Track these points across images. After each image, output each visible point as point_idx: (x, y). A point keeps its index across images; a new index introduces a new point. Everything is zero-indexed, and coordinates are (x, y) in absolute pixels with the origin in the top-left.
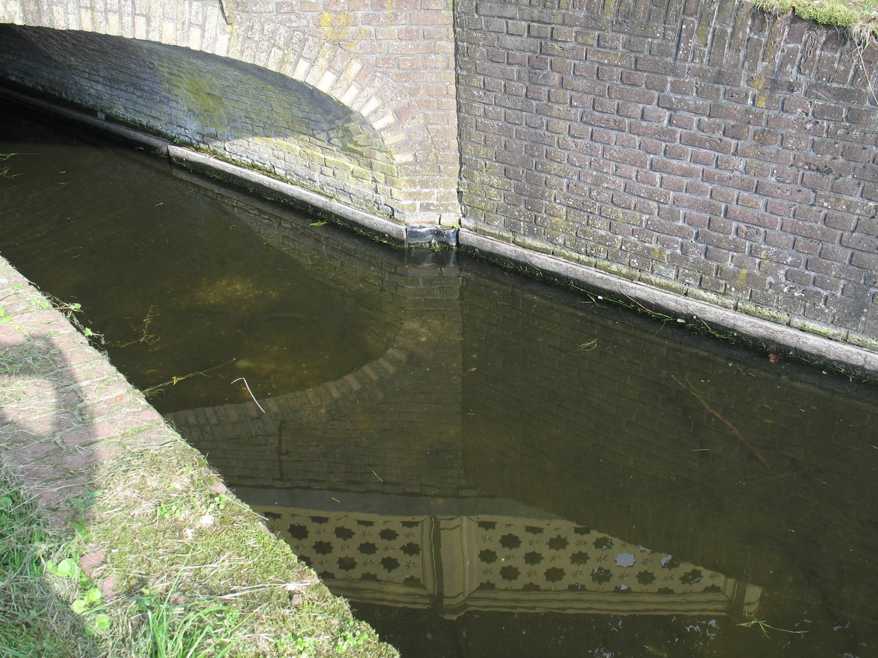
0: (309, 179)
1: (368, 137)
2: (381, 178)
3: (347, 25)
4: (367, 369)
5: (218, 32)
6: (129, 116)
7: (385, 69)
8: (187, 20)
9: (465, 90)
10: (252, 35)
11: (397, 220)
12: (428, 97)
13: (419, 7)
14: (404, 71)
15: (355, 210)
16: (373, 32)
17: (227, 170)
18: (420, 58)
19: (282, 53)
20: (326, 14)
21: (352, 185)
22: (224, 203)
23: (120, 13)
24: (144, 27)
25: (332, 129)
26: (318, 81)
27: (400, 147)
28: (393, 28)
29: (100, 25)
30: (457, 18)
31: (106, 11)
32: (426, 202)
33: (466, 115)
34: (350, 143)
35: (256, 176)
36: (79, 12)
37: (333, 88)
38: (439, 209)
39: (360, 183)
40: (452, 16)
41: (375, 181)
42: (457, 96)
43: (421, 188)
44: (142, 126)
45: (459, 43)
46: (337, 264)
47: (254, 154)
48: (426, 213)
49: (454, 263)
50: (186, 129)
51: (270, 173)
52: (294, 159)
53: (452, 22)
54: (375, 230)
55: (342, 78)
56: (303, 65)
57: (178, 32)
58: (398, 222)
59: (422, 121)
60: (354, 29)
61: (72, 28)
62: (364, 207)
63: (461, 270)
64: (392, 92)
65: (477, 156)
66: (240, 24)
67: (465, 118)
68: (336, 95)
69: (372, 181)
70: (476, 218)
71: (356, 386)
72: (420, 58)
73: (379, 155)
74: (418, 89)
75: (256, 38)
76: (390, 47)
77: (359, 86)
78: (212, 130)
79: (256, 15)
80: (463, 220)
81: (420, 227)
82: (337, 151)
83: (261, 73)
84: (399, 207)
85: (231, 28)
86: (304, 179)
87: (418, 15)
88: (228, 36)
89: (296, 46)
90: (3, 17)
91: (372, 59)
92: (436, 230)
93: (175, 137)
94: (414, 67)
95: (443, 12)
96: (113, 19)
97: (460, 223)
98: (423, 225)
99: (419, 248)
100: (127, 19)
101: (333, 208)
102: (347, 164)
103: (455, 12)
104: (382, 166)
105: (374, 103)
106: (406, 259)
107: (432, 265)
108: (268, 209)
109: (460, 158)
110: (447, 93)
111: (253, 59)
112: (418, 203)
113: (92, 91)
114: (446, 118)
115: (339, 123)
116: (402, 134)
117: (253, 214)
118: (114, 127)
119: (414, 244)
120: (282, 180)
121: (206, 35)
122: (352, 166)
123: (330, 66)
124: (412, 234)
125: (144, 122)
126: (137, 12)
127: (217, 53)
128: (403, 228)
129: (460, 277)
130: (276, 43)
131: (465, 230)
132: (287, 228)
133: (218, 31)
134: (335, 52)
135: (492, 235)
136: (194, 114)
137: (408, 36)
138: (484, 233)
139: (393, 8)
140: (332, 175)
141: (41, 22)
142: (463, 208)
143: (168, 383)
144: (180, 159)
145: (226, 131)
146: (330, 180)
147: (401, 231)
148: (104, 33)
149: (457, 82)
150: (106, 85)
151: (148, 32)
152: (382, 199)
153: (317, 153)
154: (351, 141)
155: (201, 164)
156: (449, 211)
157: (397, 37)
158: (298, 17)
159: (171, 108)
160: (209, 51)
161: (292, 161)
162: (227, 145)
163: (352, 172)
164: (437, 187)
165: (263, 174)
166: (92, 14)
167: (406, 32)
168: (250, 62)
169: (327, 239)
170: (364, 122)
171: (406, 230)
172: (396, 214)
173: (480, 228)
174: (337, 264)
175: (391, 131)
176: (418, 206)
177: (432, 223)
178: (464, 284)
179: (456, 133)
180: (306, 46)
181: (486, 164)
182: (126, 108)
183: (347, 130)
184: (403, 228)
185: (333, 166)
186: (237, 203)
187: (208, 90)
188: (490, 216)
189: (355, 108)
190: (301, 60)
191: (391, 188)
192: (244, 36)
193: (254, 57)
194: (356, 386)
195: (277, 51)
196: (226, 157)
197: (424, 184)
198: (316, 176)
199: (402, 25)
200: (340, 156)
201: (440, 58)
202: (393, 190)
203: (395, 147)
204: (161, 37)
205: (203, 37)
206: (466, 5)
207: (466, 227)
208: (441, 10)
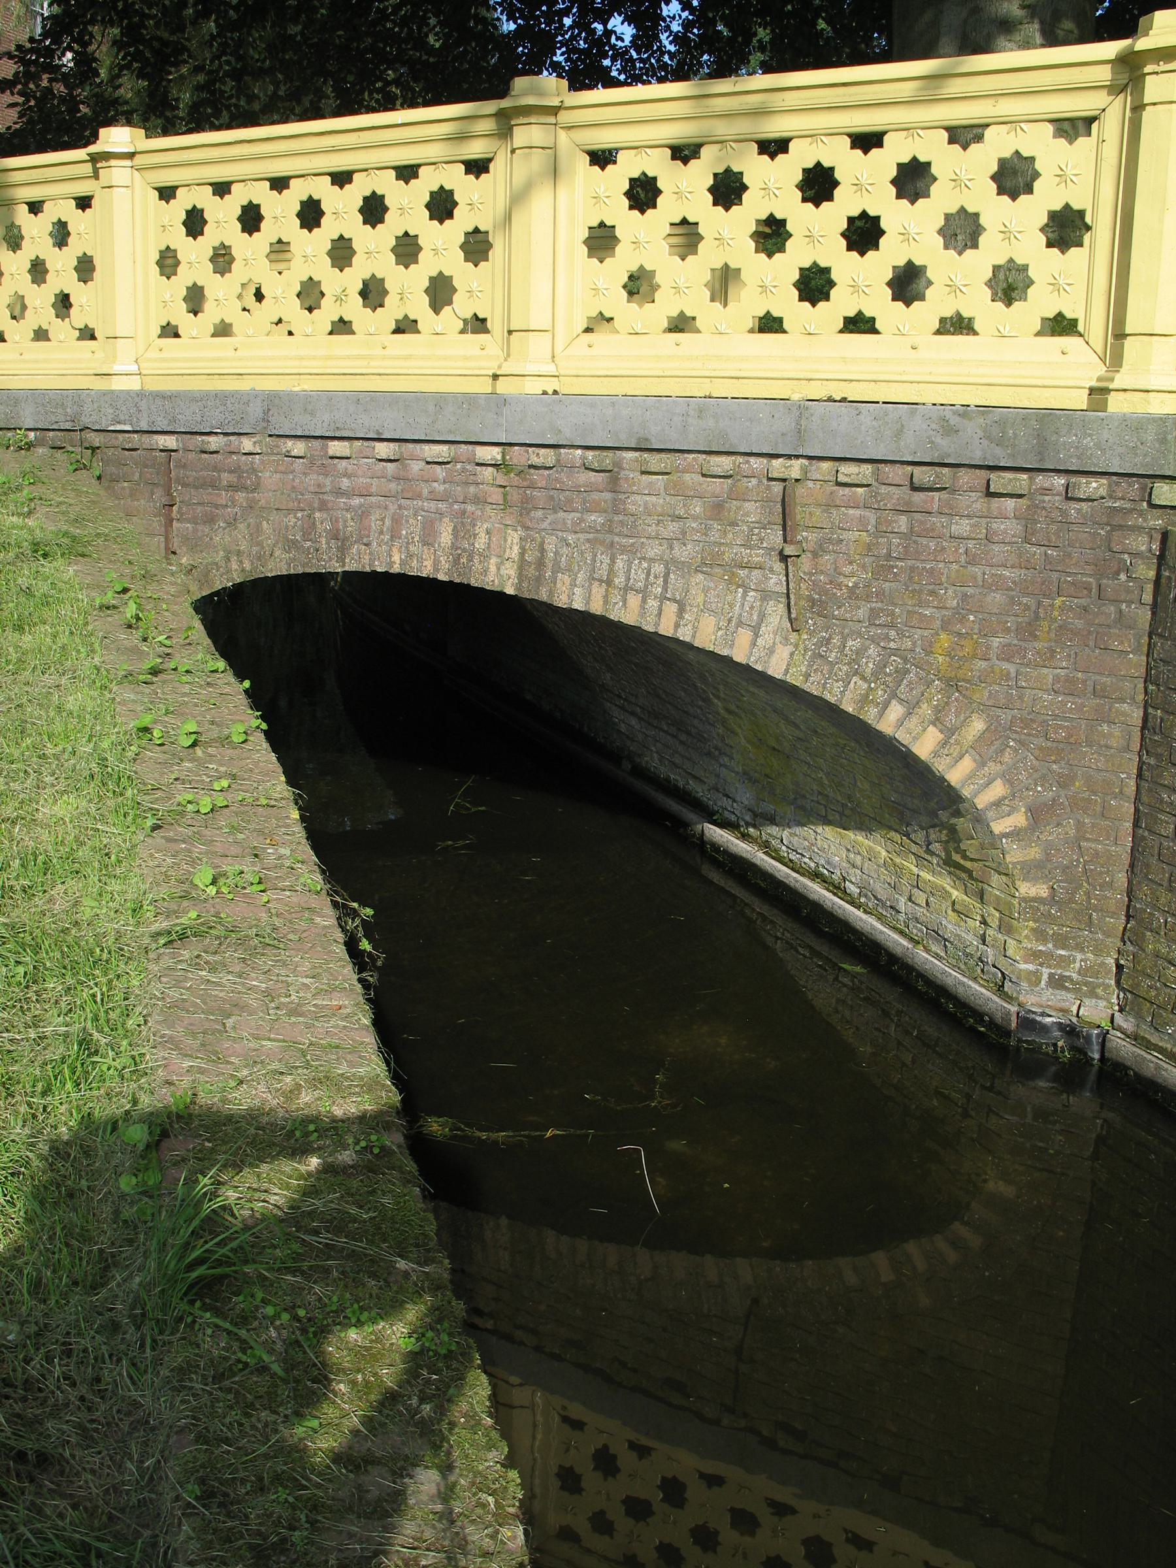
0: (891, 907)
1: (982, 847)
2: (994, 917)
3: (974, 656)
4: (911, 1247)
5: (777, 640)
6: (663, 771)
7: (1023, 737)
8: (736, 616)
9: (1150, 790)
10: (826, 652)
11: (1006, 994)
12: (1087, 793)
13: (1092, 644)
14: (1055, 745)
15: (946, 969)
16: (1013, 675)
17: (777, 875)
18: (1083, 726)
19: (865, 686)
20: (943, 636)
21: (950, 925)
22: (765, 930)
23: (644, 593)
24: (674, 618)
25: (933, 826)
26: (915, 739)
27: (1031, 870)
28: (1045, 671)
29: (614, 606)
30: (1151, 669)
31: (627, 589)
32: (1059, 972)
33: (1146, 834)
34: (957, 853)
35: (817, 891)
36: (591, 584)
37: (936, 754)
38: (1080, 989)
39: (962, 924)
40: (1145, 664)
41: (984, 922)
42: (1136, 799)
43: (1054, 946)
44: (676, 788)
45: (1150, 710)
46: (908, 1058)
47: (821, 853)
48: (1058, 992)
49: (1092, 1091)
50: (734, 801)
51: (838, 889)
52: (875, 870)
53: (1144, 676)
54: (972, 1008)
55: (952, 741)
56: (895, 711)
57: (720, 633)
58: (1008, 998)
59: (1072, 833)
60: (984, 664)
61: (576, 606)
62: (963, 967)
63: (1102, 1106)
64: (1031, 775)
65: (1155, 907)
66: (812, 634)
67: (1143, 838)
68: (940, 766)
69: (981, 923)
70: (1139, 1017)
71: (887, 1275)
72: (1083, 726)
73: (995, 879)
74: (1072, 778)
75: (832, 657)
76: (1037, 702)
77: (977, 757)
78: (770, 808)
79: (837, 622)
80: (1117, 1014)
81: (1043, 1014)
82: (938, 865)
83: (832, 712)
84: (1012, 972)
85: (797, 637)
86: (884, 905)
87: (1088, 655)
88: (791, 648)
89: (890, 679)
90: (493, 581)
91: (1005, 716)
92: (1068, 1026)
93: (718, 812)
94: (1072, 740)
95: (1131, 656)
96: (634, 600)
97: (1112, 1021)
98: (1048, 1011)
99: (1035, 1049)
100: (652, 603)
101: (916, 960)
102: (948, 888)
103: (1150, 659)
104: (997, 897)
105: (998, 790)
106: (1010, 1065)
107: (1053, 1087)
108: (825, 949)
109: (1128, 907)
110: (1121, 792)
111: (821, 689)
112: (1046, 972)
113: (623, 727)
114: (1113, 834)
115: (943, 815)
116: (1036, 849)
117: (802, 955)
118: (639, 785)
119: (1027, 1042)
120: (852, 903)
121: (760, 641)
122: (955, 894)
123: (937, 719)
124: (1028, 1023)
125: (681, 784)
126: (668, 596)
127: (770, 672)
128: (1013, 1009)
129: (1099, 1118)
130: (861, 670)
131: (1119, 1034)
132: (845, 985)
133: (778, 639)
134: (949, 698)
135: (1161, 1050)
136: (750, 779)
137: (1069, 688)
138: (1148, 1046)
139: (1050, 640)
140: (924, 905)
141: (538, 594)
142: (1122, 995)
143: (538, 1133)
144: (716, 847)
145: (789, 810)
146: (920, 912)
147: (1008, 1013)
148: (616, 620)
149: (1140, 776)
150: (643, 719)
151: (677, 626)
152: (990, 954)
153: (909, 865)
154: (958, 850)
155: (741, 858)
156: (1097, 997)
157: (1050, 686)
158: (901, 635)
159: (721, 765)
160: (759, 668)
161: (872, 875)
162: (785, 834)
163: (954, 903)
164: (1082, 950)
165: (828, 890)
166: (607, 591)
167: (1066, 681)
168: (815, 693)
169: (899, 1013)
170: (979, 819)
171: (1018, 1014)
172: (1007, 984)
173: (1142, 1034)
174: (908, 1058)
175: (1019, 840)
176: (1045, 977)
177: (1065, 1011)
178: (1104, 1133)
179: (1127, 862)
180: (905, 681)
181: (1166, 922)
182: (661, 759)
183: (953, 830)
184: (1013, 1009)
185: (928, 889)
186: (783, 934)
187: (773, 743)
188: (1162, 1016)
189: (966, 792)
190: (894, 702)
191: (1006, 938)
192: (814, 652)
193: (824, 688)
194: (887, 1275)
195: (860, 682)
196: (782, 853)
197: (1061, 941)
198: (902, 903)
199: (1062, 667)
200: (940, 873)
201: (1117, 731)
202: (1009, 941)
203: (1022, 869)
204: (694, 636)
205: (755, 644)
206: (1166, 647)
207: (1120, 1029)
208: (1128, 653)
